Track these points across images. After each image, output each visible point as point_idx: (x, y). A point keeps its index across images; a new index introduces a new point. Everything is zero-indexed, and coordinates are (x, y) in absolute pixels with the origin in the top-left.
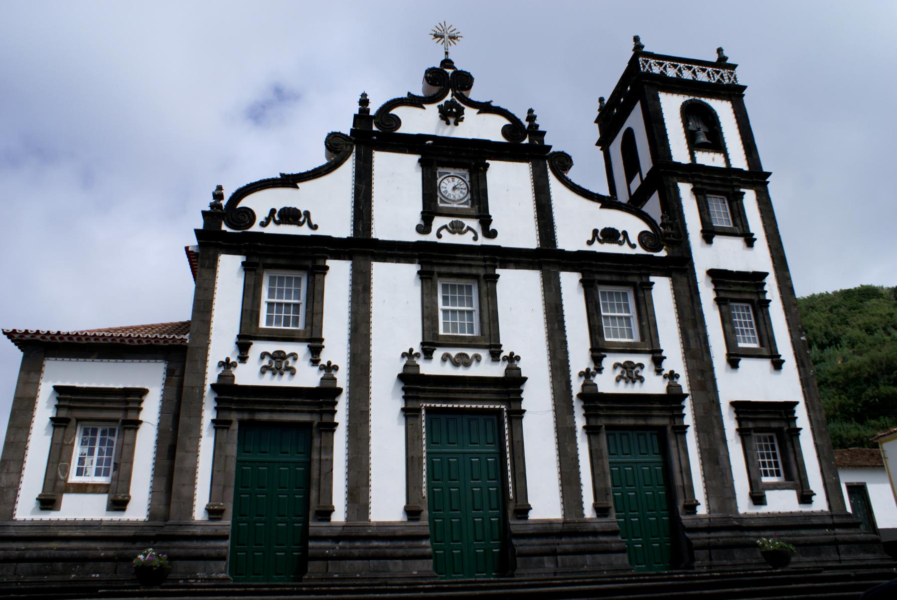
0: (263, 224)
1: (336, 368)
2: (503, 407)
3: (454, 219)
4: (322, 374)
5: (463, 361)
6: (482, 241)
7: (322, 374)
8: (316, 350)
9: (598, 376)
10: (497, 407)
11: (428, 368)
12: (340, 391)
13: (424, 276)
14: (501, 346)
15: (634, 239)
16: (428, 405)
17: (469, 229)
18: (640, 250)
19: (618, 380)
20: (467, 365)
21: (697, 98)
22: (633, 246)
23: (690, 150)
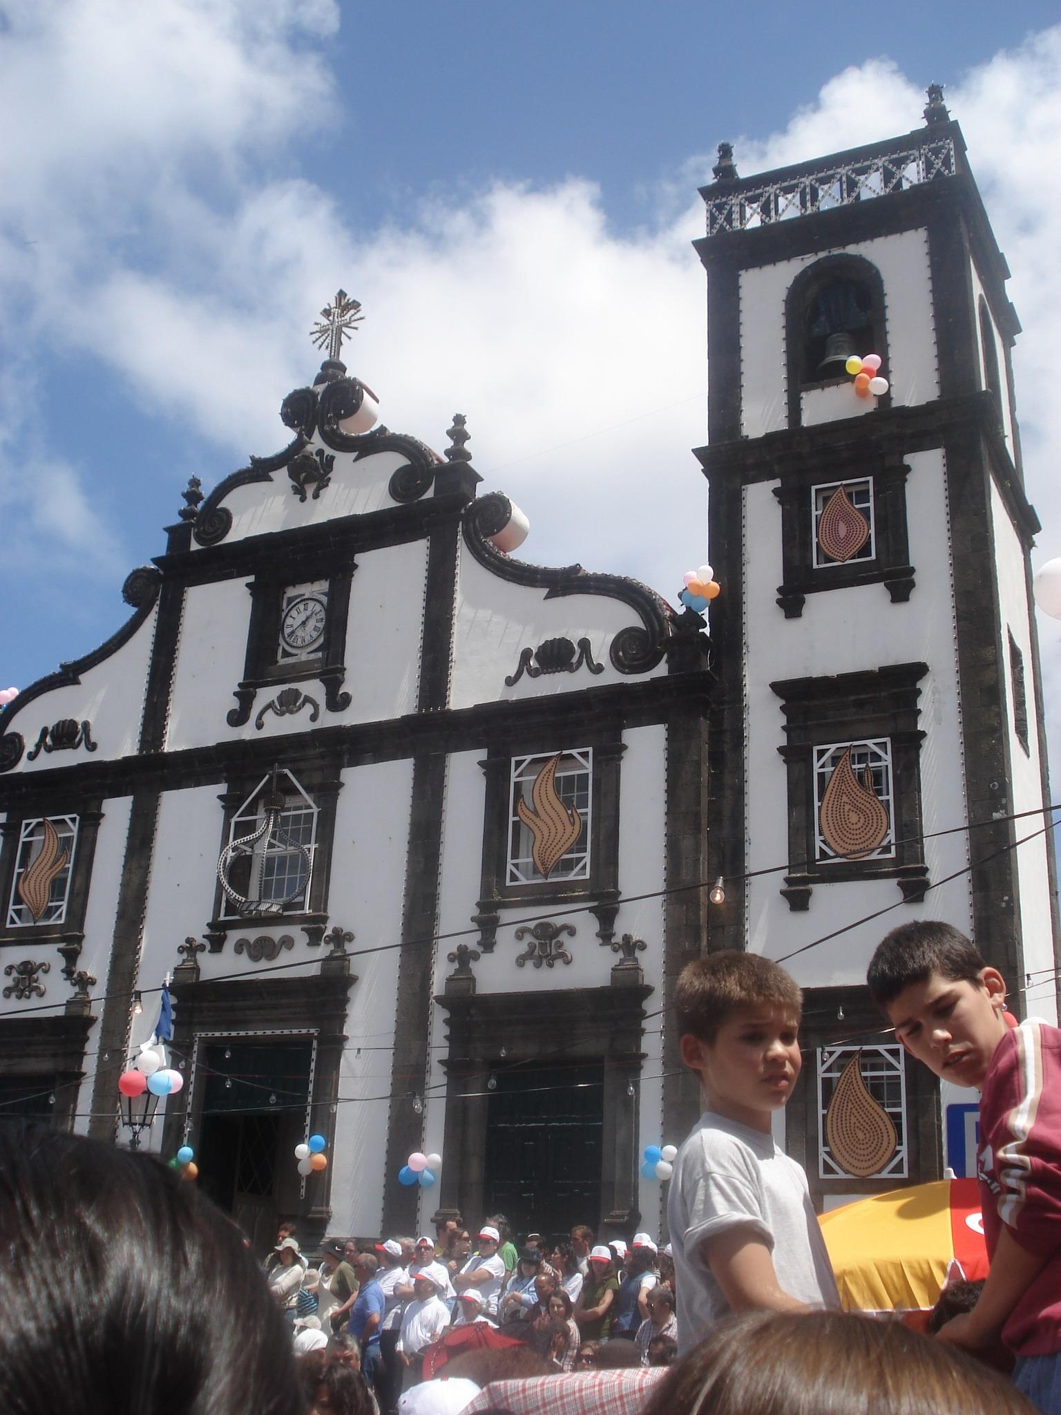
0: (32, 757)
1: (642, 946)
2: (312, 1031)
3: (285, 687)
4: (616, 958)
5: (264, 950)
6: (329, 720)
7: (616, 958)
8: (71, 956)
9: (485, 958)
10: (304, 1031)
11: (216, 966)
12: (91, 1021)
13: (230, 803)
14: (927, 869)
15: (601, 654)
16: (203, 1035)
17: (308, 700)
18: (612, 677)
19: (521, 961)
20: (271, 956)
21: (836, 251)
22: (598, 669)
23: (789, 397)
